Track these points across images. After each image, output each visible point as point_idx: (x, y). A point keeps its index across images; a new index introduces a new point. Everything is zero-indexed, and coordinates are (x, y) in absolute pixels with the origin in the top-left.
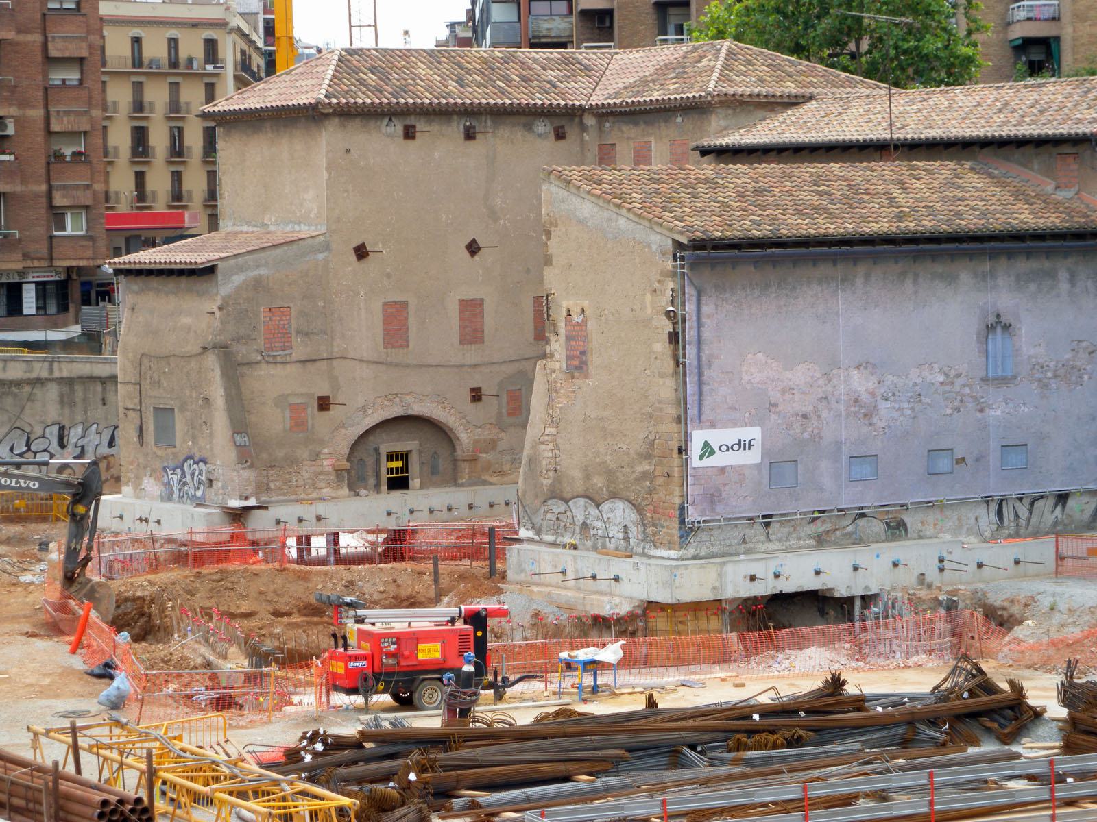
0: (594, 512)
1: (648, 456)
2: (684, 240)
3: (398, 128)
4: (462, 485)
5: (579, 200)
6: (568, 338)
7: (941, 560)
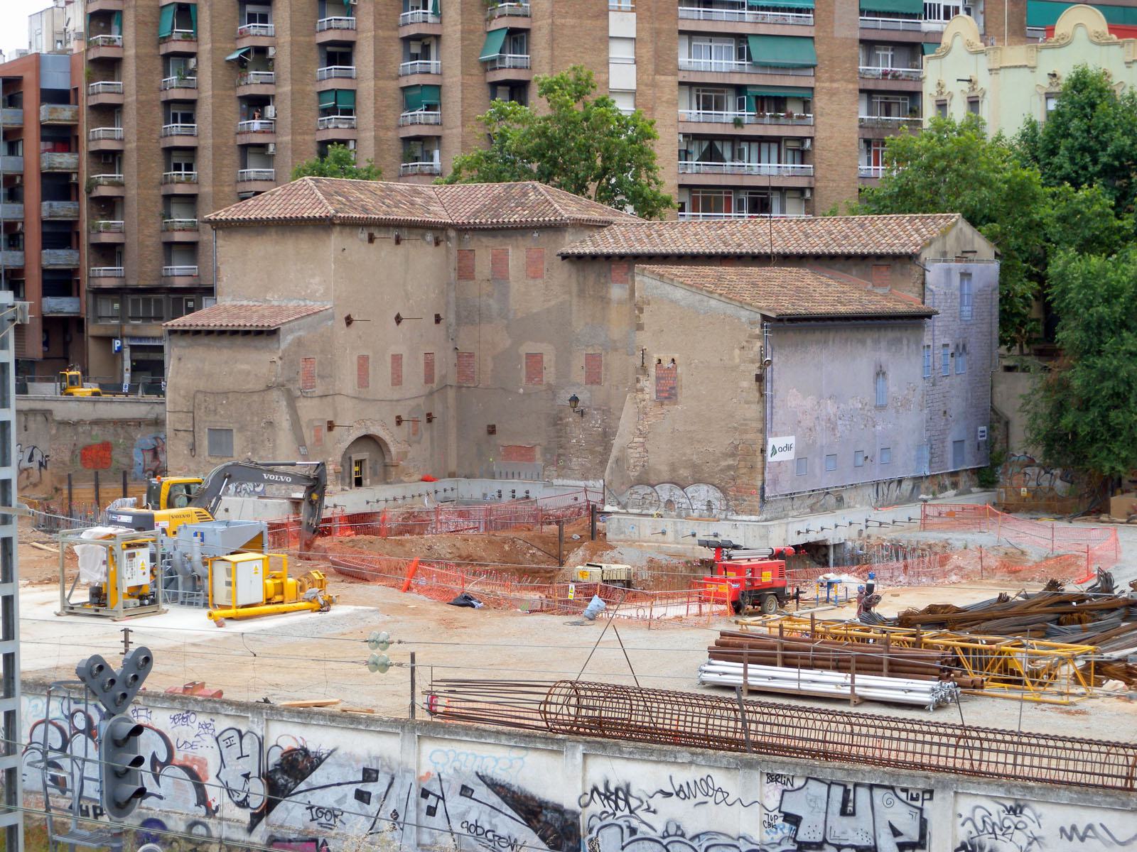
0: (678, 492)
1: (733, 455)
2: (773, 315)
3: (364, 235)
4: (391, 483)
5: (672, 287)
6: (658, 378)
7: (867, 521)
